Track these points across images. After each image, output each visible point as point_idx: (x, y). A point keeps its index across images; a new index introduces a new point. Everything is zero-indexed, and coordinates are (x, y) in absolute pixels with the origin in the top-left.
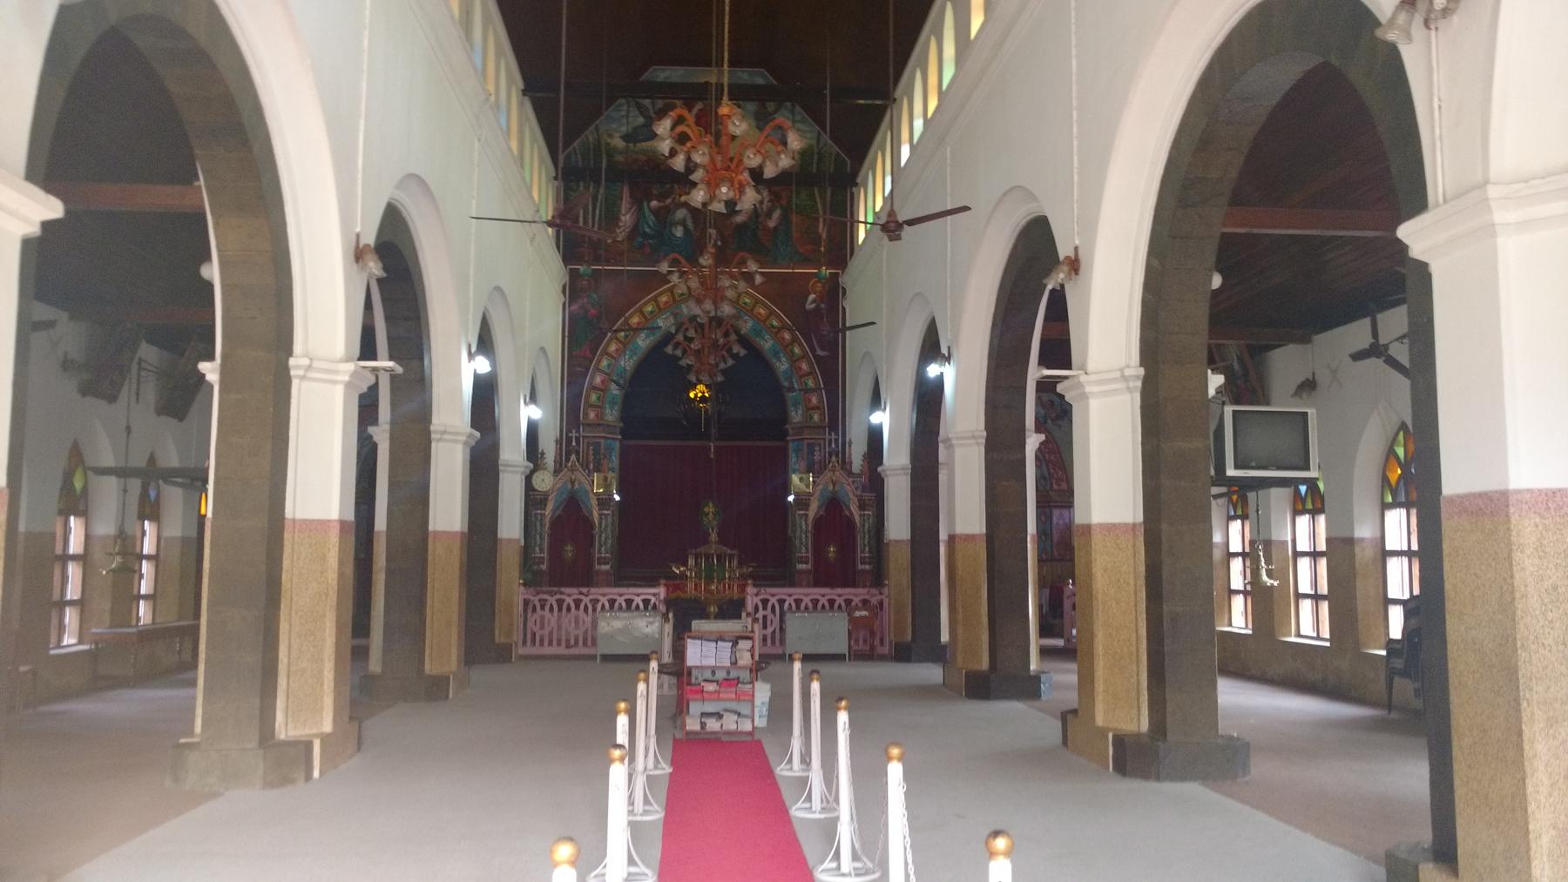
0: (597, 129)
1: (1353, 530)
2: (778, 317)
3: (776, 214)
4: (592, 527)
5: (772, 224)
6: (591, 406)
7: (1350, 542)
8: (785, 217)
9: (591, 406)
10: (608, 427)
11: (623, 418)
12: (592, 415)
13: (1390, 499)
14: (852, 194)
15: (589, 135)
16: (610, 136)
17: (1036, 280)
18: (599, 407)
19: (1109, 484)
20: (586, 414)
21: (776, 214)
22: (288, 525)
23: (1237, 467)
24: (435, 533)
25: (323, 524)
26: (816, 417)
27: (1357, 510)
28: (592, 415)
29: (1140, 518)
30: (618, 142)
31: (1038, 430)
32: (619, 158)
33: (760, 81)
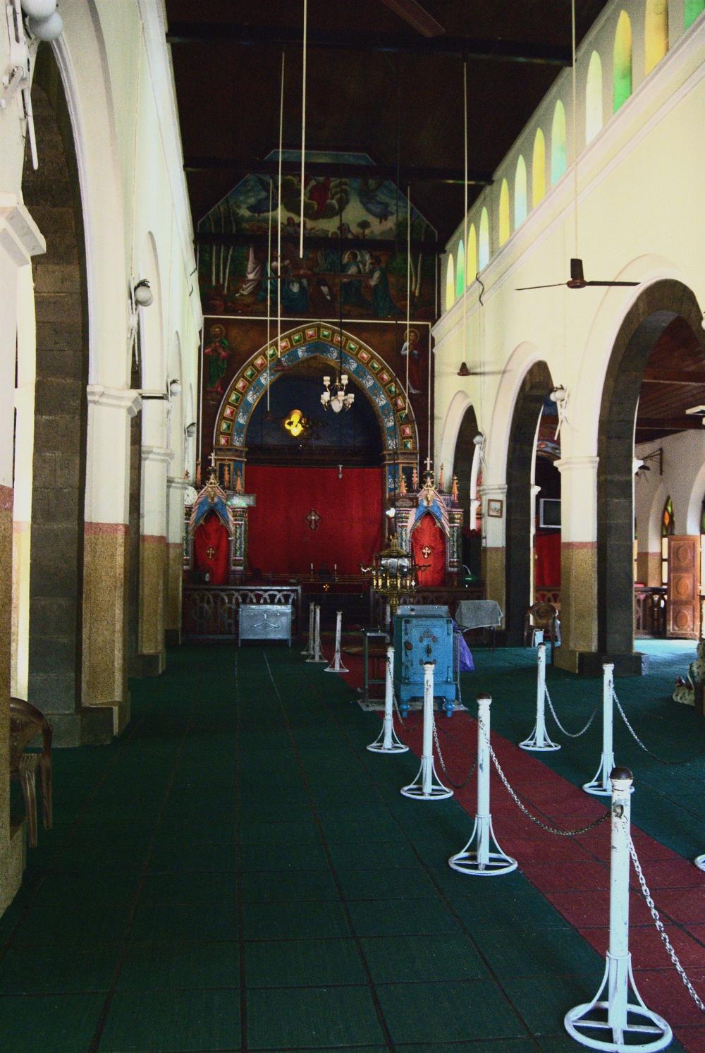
0: (227, 202)
1: (647, 547)
2: (378, 360)
3: (377, 275)
4: (228, 533)
5: (373, 283)
6: (222, 433)
7: (646, 554)
8: (383, 278)
9: (222, 433)
10: (237, 452)
11: (247, 444)
12: (223, 441)
13: (665, 533)
14: (439, 260)
15: (220, 206)
16: (239, 207)
17: (536, 400)
18: (228, 434)
19: (579, 521)
20: (218, 441)
21: (377, 275)
22: (562, 544)
23: (544, 524)
24: (565, 543)
25: (114, 527)
26: (409, 445)
27: (650, 537)
28: (223, 441)
29: (595, 540)
30: (244, 212)
31: (537, 484)
32: (245, 225)
33: (363, 163)
